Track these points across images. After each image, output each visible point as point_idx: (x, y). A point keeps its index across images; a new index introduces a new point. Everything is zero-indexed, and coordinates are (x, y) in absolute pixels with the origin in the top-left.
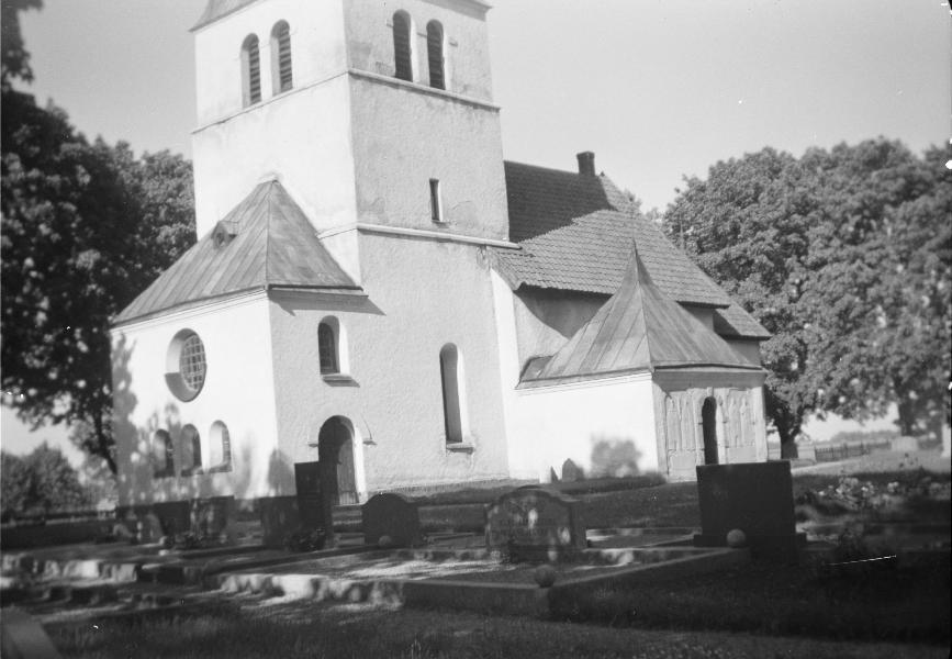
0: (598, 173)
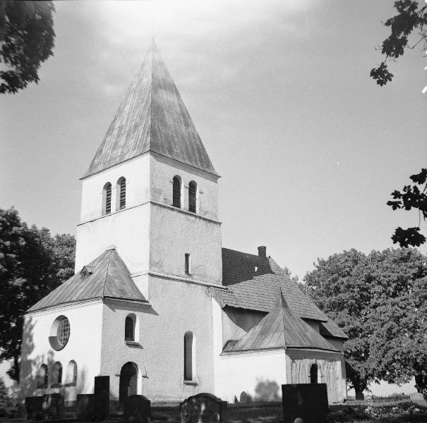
0: (267, 256)
